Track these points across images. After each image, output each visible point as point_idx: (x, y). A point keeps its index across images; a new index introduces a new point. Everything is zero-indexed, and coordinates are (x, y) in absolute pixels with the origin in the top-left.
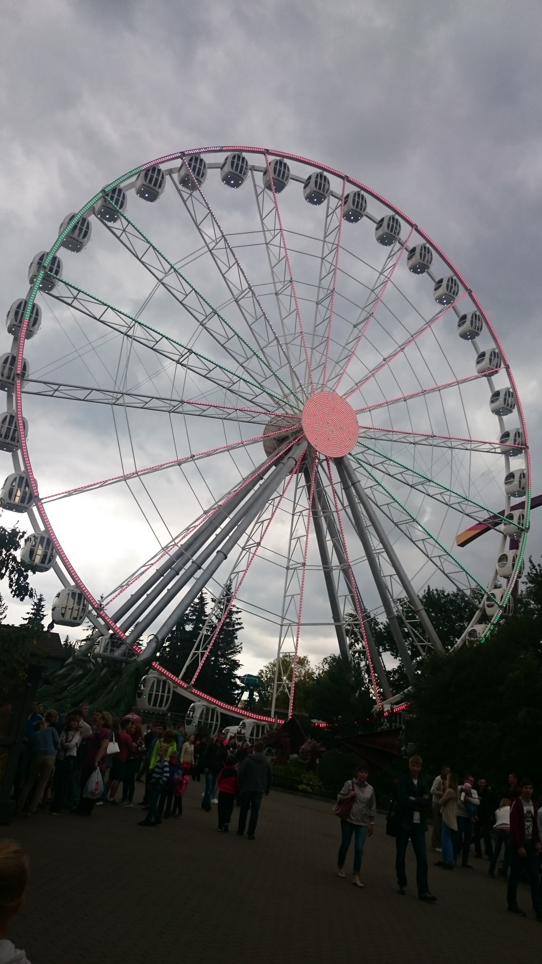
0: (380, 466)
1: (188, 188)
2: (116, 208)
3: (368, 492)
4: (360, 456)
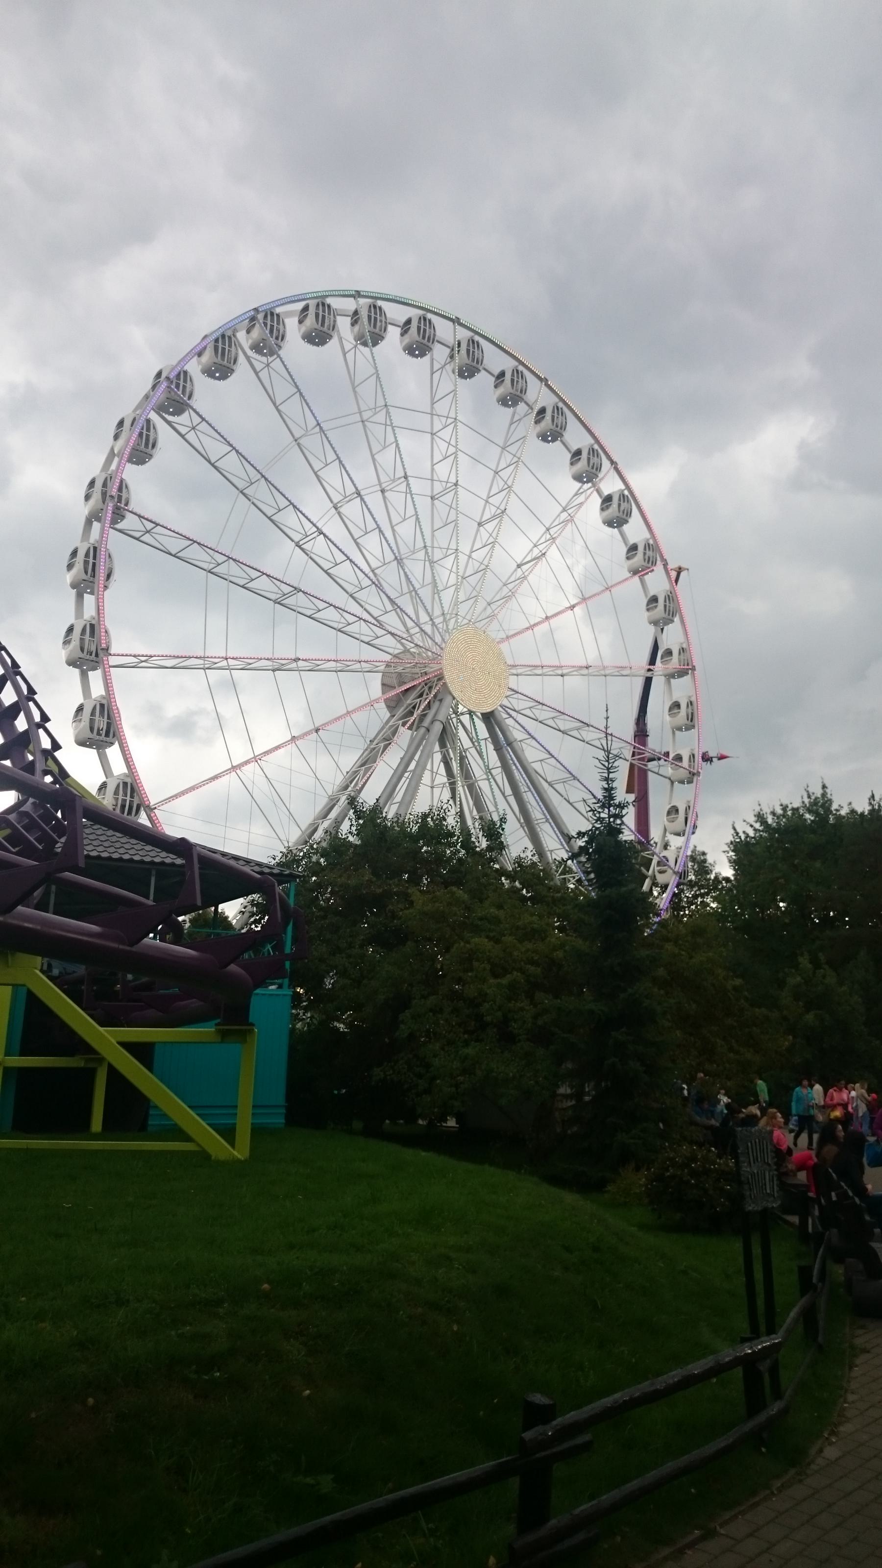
0: (351, 619)
1: (265, 355)
2: (182, 399)
3: (537, 766)
4: (380, 632)
